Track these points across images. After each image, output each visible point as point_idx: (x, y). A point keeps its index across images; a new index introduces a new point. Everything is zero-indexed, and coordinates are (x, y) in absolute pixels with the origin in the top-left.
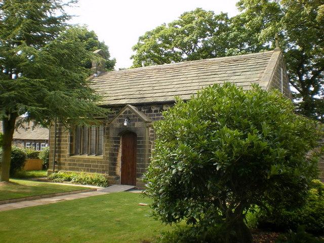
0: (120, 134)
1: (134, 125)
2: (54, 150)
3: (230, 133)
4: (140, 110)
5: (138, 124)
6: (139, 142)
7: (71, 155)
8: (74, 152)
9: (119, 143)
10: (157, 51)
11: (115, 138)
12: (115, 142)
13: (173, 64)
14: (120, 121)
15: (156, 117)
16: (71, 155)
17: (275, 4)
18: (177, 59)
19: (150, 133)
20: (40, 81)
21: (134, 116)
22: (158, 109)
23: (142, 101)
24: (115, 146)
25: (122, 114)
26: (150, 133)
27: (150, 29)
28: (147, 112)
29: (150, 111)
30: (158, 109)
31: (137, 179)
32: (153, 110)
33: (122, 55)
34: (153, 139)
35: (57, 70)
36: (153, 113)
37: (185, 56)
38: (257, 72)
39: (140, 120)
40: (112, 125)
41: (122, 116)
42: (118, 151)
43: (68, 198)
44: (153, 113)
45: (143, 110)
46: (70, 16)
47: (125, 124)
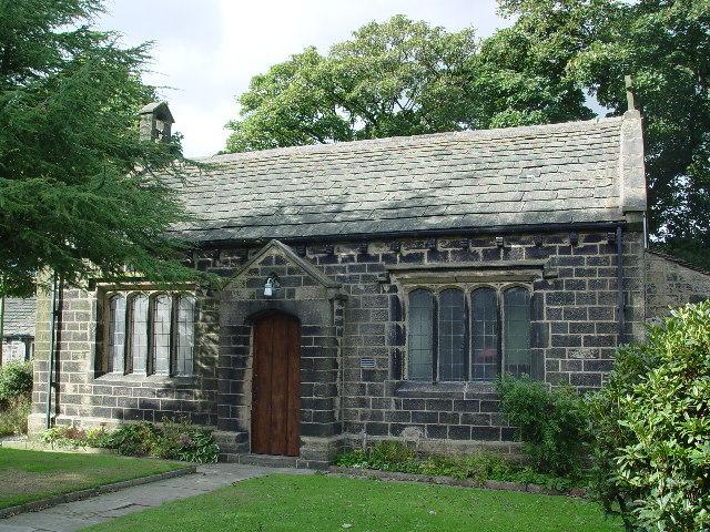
0: (251, 319)
1: (292, 294)
3: (59, 511)
4: (303, 255)
5: (301, 293)
6: (309, 341)
7: (97, 375)
8: (105, 367)
9: (246, 342)
10: (305, 107)
11: (234, 330)
12: (237, 341)
13: (332, 145)
14: (250, 283)
16: (97, 375)
17: (132, 57)
18: (343, 133)
21: (291, 271)
23: (309, 231)
24: (237, 351)
25: (256, 265)
26: (336, 317)
28: (322, 260)
29: (332, 258)
33: (203, 130)
34: (340, 333)
35: (574, 40)
37: (360, 124)
41: (255, 271)
42: (244, 365)
45: (312, 257)
46: (137, 51)
47: (268, 292)
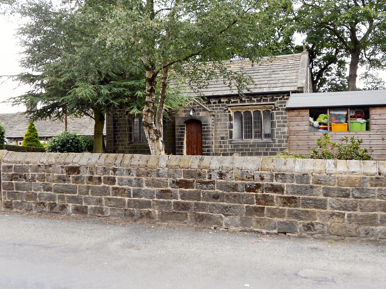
0: (185, 122)
1: (198, 114)
2: (113, 139)
5: (202, 114)
15: (215, 108)
19: (212, 121)
20: (321, 213)
21: (198, 107)
22: (217, 101)
27: (111, 237)
28: (206, 103)
29: (209, 103)
30: (217, 101)
31: (94, 134)
32: (212, 102)
36: (212, 104)
38: (293, 71)
39: (204, 110)
40: (178, 115)
43: (192, 170)
44: (212, 104)
